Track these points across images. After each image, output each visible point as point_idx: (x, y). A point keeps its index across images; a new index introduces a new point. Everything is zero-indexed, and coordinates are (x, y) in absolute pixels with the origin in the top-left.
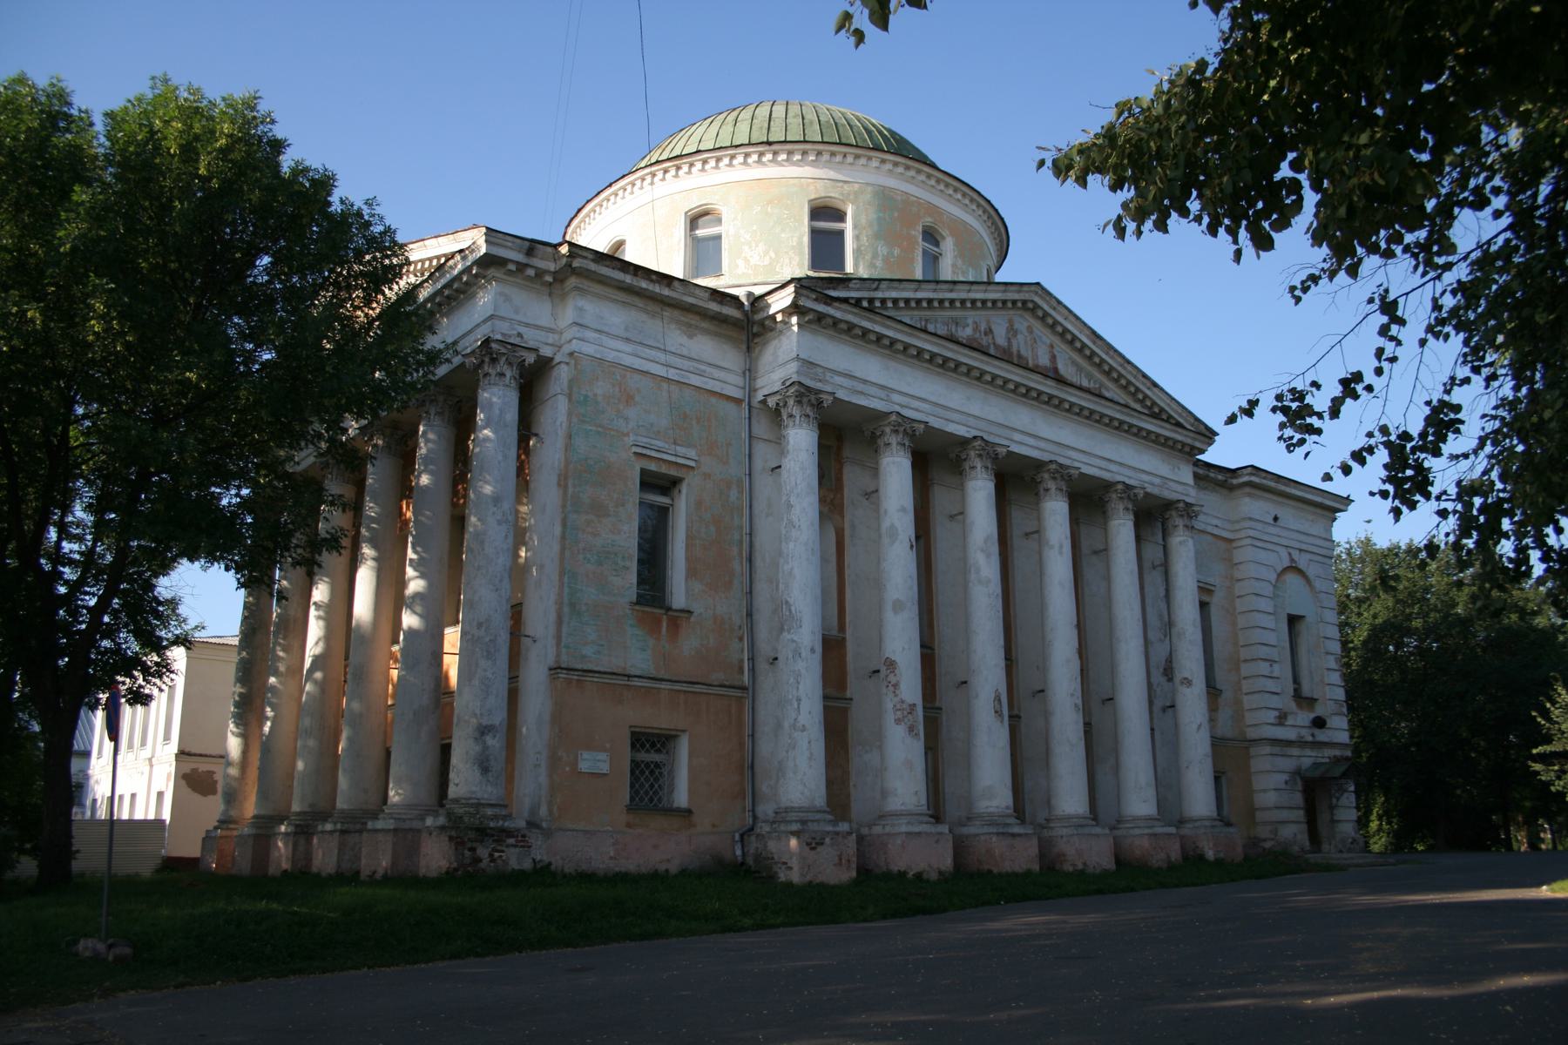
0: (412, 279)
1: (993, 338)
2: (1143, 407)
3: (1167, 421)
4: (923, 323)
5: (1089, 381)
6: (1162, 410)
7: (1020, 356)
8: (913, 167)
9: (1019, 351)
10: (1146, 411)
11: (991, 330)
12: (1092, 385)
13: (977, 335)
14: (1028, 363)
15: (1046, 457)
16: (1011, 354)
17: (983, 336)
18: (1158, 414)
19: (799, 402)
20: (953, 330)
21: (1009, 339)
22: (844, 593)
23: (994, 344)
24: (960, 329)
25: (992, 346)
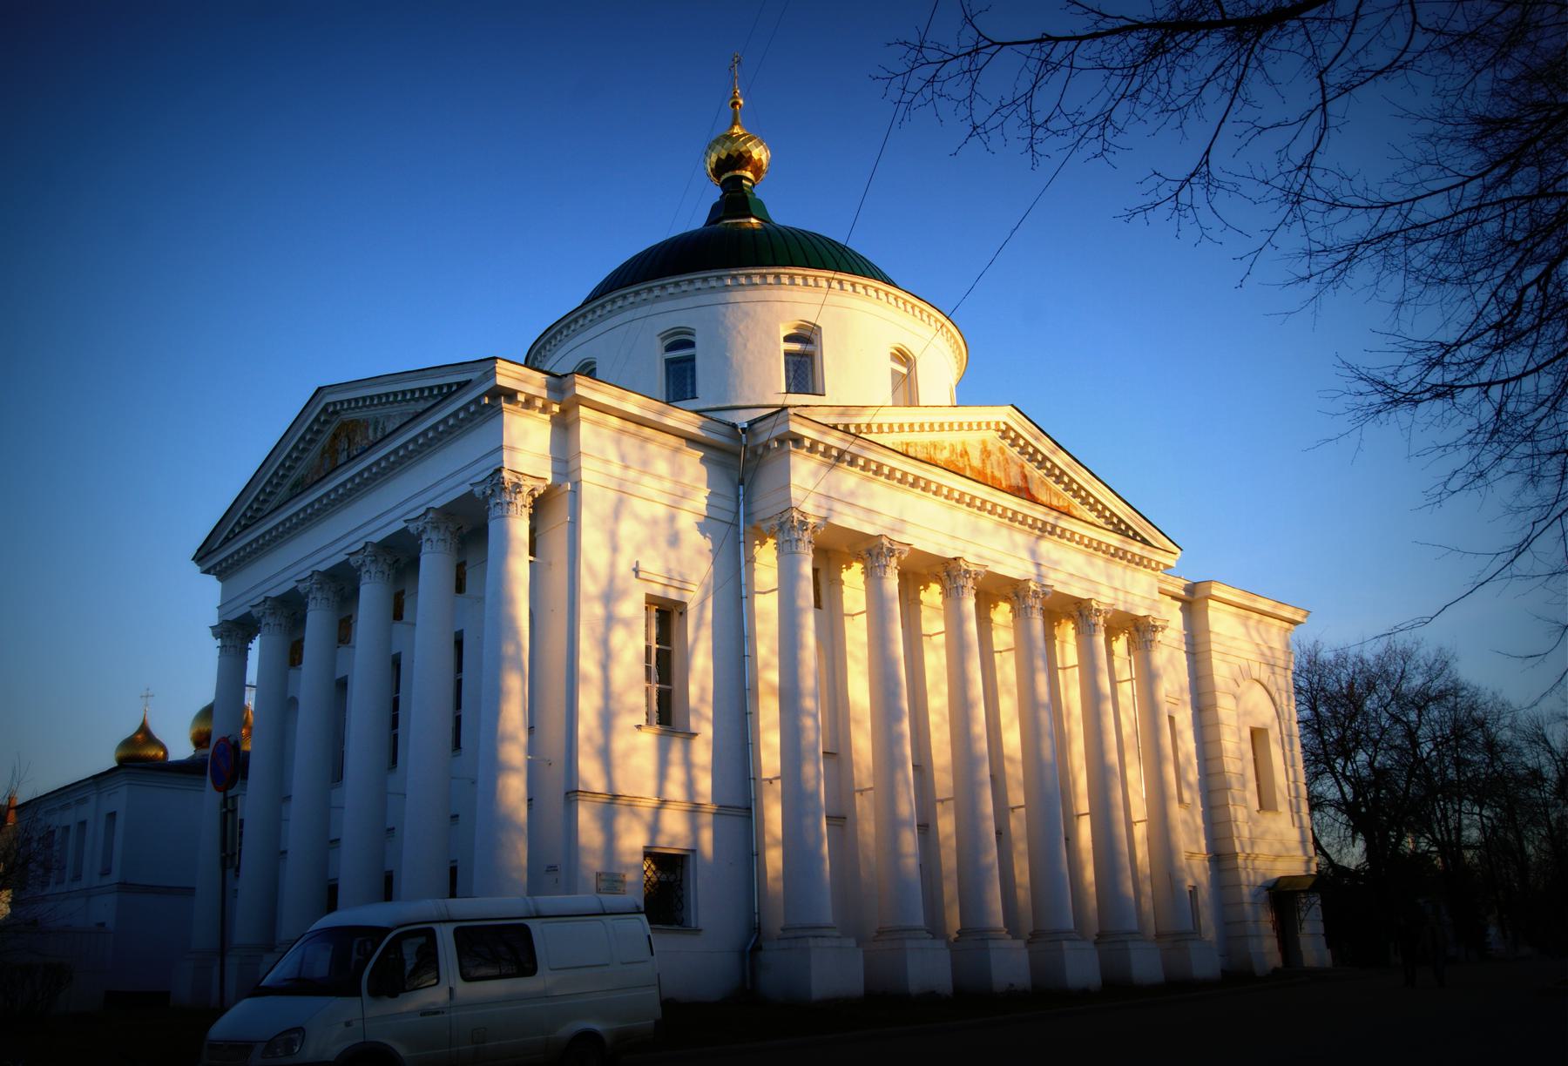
0: (1543, 760)
1: (969, 459)
2: (435, 399)
3: (1133, 538)
4: (905, 447)
5: (1058, 500)
6: (1128, 527)
7: (993, 477)
8: (607, 302)
9: (992, 472)
10: (440, 398)
11: (966, 452)
12: (1061, 503)
13: (954, 458)
14: (1001, 483)
16: (985, 475)
17: (959, 458)
18: (446, 393)
19: (1519, 748)
20: (932, 452)
21: (983, 460)
22: (1135, 849)
23: (970, 466)
24: (938, 451)
25: (968, 467)
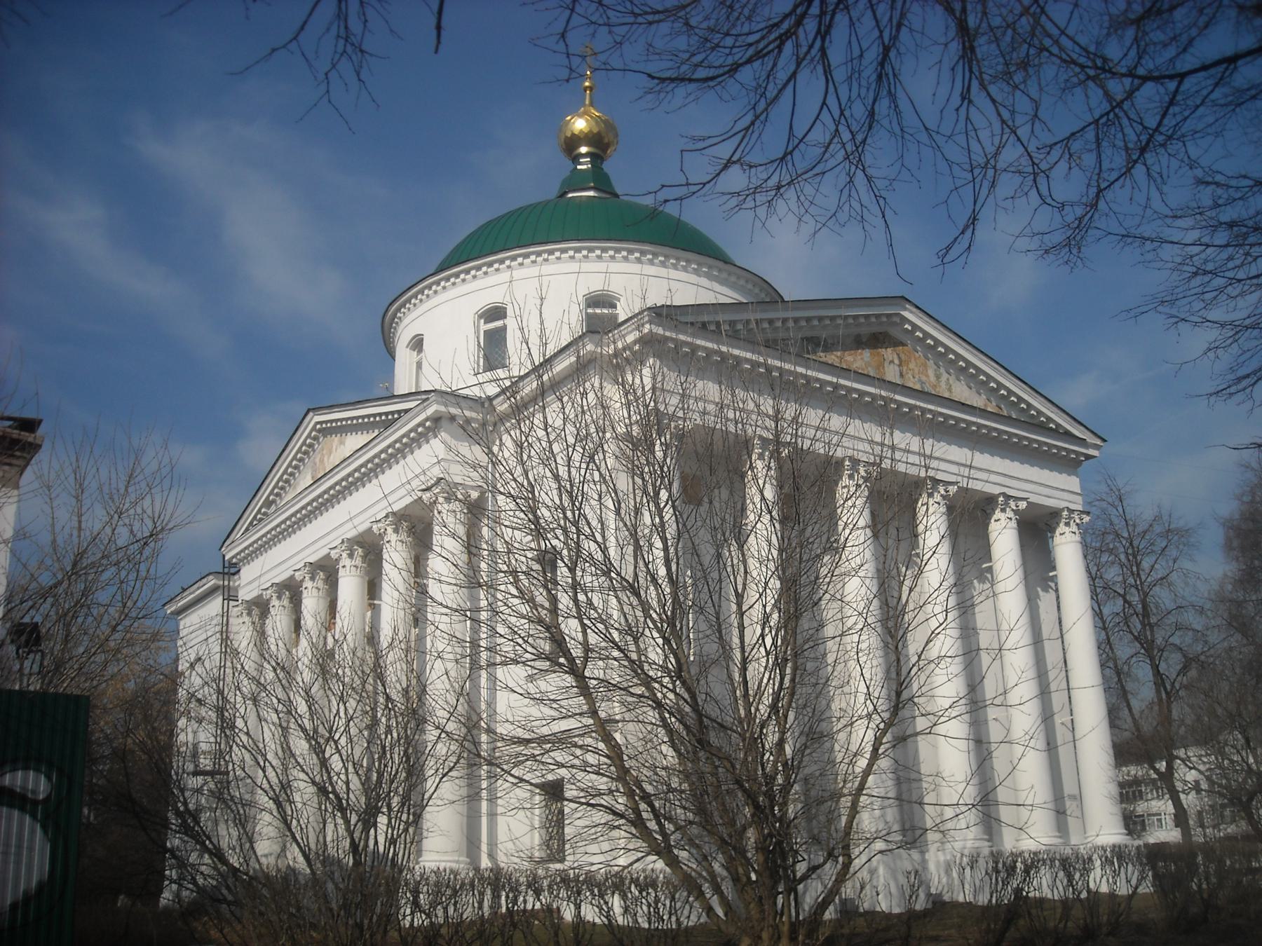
15: (996, 490)
